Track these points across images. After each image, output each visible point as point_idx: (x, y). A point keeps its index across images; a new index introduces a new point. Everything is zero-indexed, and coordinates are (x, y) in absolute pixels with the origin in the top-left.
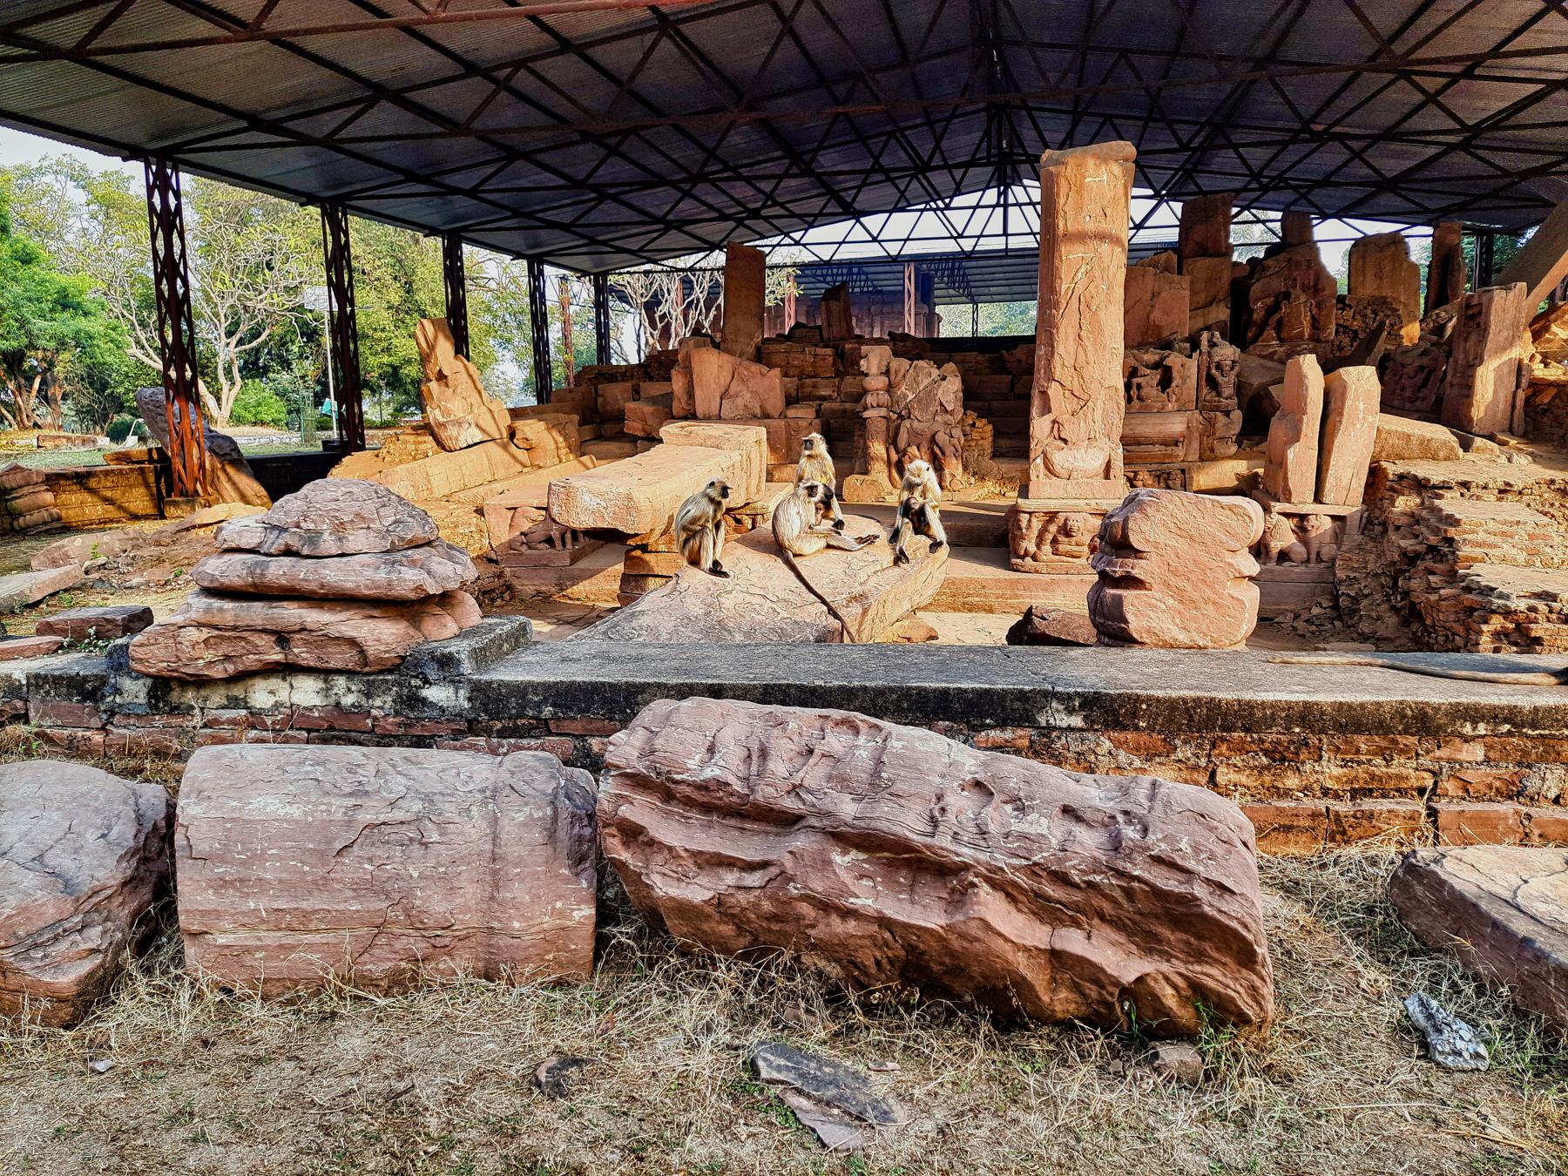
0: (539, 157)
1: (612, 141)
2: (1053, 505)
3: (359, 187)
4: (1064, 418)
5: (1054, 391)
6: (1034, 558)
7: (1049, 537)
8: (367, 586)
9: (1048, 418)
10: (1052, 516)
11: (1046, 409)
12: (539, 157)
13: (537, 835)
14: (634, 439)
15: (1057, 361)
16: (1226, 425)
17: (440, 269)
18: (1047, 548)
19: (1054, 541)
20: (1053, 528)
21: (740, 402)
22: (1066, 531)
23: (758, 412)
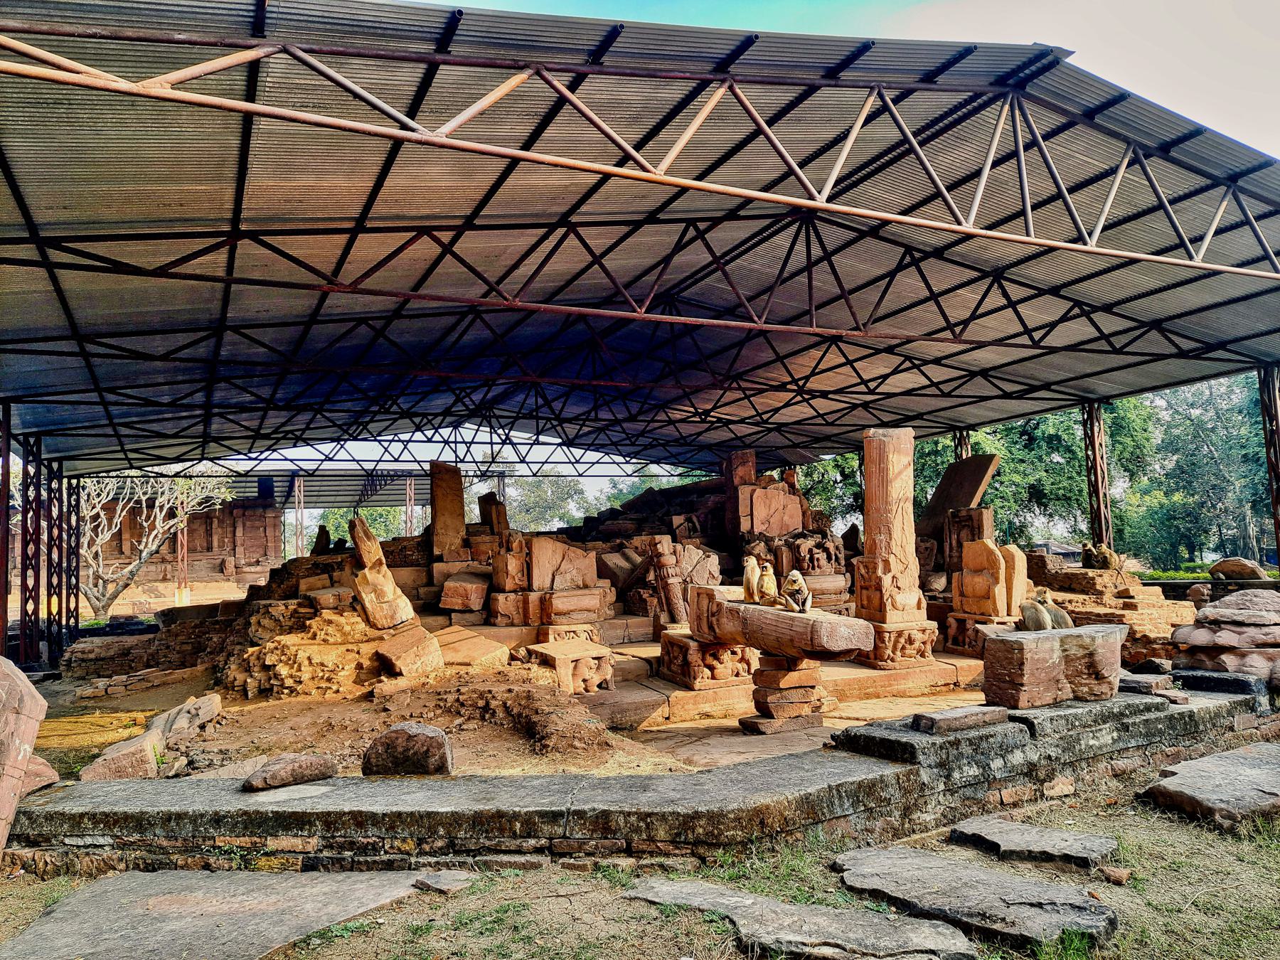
0: (980, 311)
1: (917, 362)
2: (901, 626)
3: (87, 451)
4: (898, 575)
5: (892, 559)
6: (893, 660)
7: (900, 646)
8: (191, 889)
9: (889, 576)
10: (900, 634)
11: (887, 569)
12: (1033, 292)
13: (396, 535)
14: (447, 613)
15: (893, 543)
17: (504, 808)
18: (899, 653)
19: (903, 648)
20: (902, 640)
21: (568, 577)
22: (910, 641)
23: (581, 583)
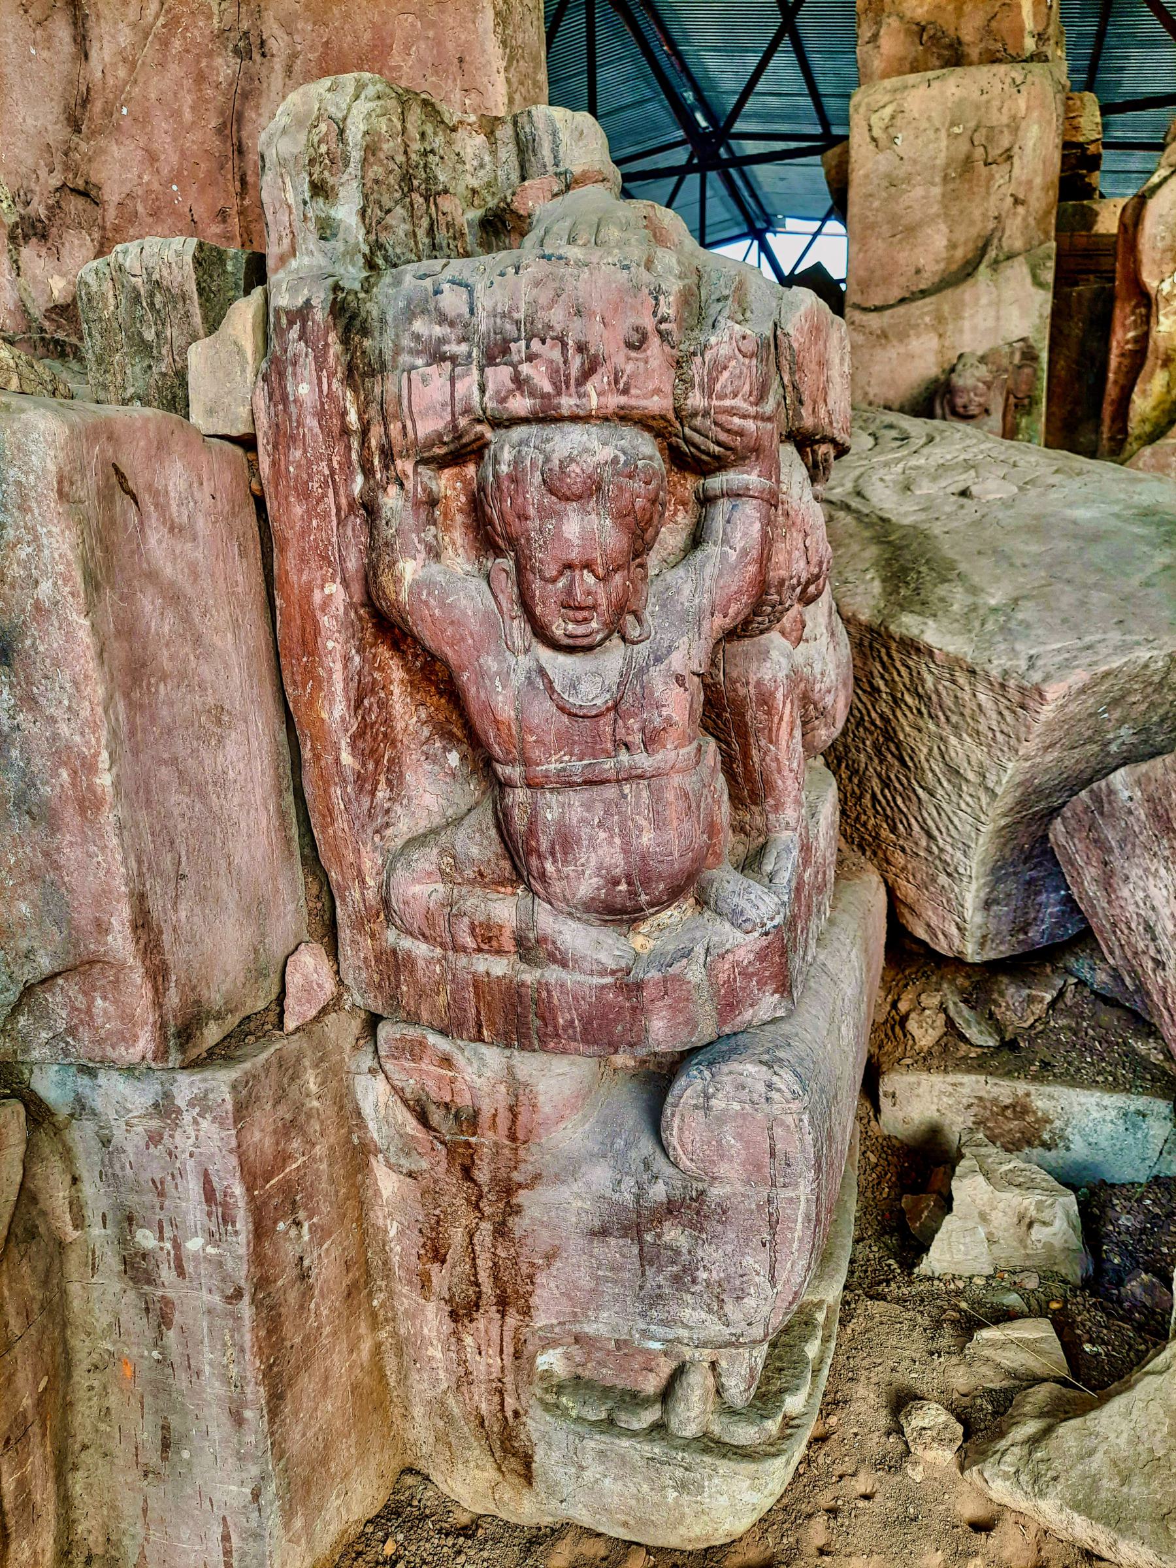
16: (634, 1224)
